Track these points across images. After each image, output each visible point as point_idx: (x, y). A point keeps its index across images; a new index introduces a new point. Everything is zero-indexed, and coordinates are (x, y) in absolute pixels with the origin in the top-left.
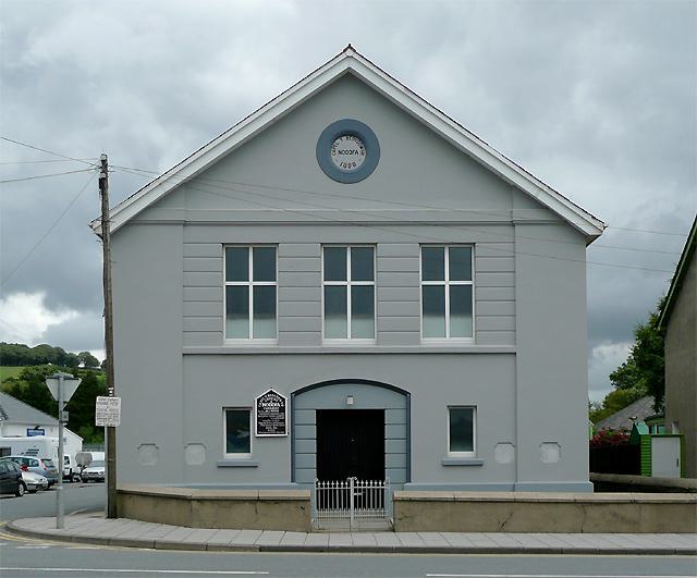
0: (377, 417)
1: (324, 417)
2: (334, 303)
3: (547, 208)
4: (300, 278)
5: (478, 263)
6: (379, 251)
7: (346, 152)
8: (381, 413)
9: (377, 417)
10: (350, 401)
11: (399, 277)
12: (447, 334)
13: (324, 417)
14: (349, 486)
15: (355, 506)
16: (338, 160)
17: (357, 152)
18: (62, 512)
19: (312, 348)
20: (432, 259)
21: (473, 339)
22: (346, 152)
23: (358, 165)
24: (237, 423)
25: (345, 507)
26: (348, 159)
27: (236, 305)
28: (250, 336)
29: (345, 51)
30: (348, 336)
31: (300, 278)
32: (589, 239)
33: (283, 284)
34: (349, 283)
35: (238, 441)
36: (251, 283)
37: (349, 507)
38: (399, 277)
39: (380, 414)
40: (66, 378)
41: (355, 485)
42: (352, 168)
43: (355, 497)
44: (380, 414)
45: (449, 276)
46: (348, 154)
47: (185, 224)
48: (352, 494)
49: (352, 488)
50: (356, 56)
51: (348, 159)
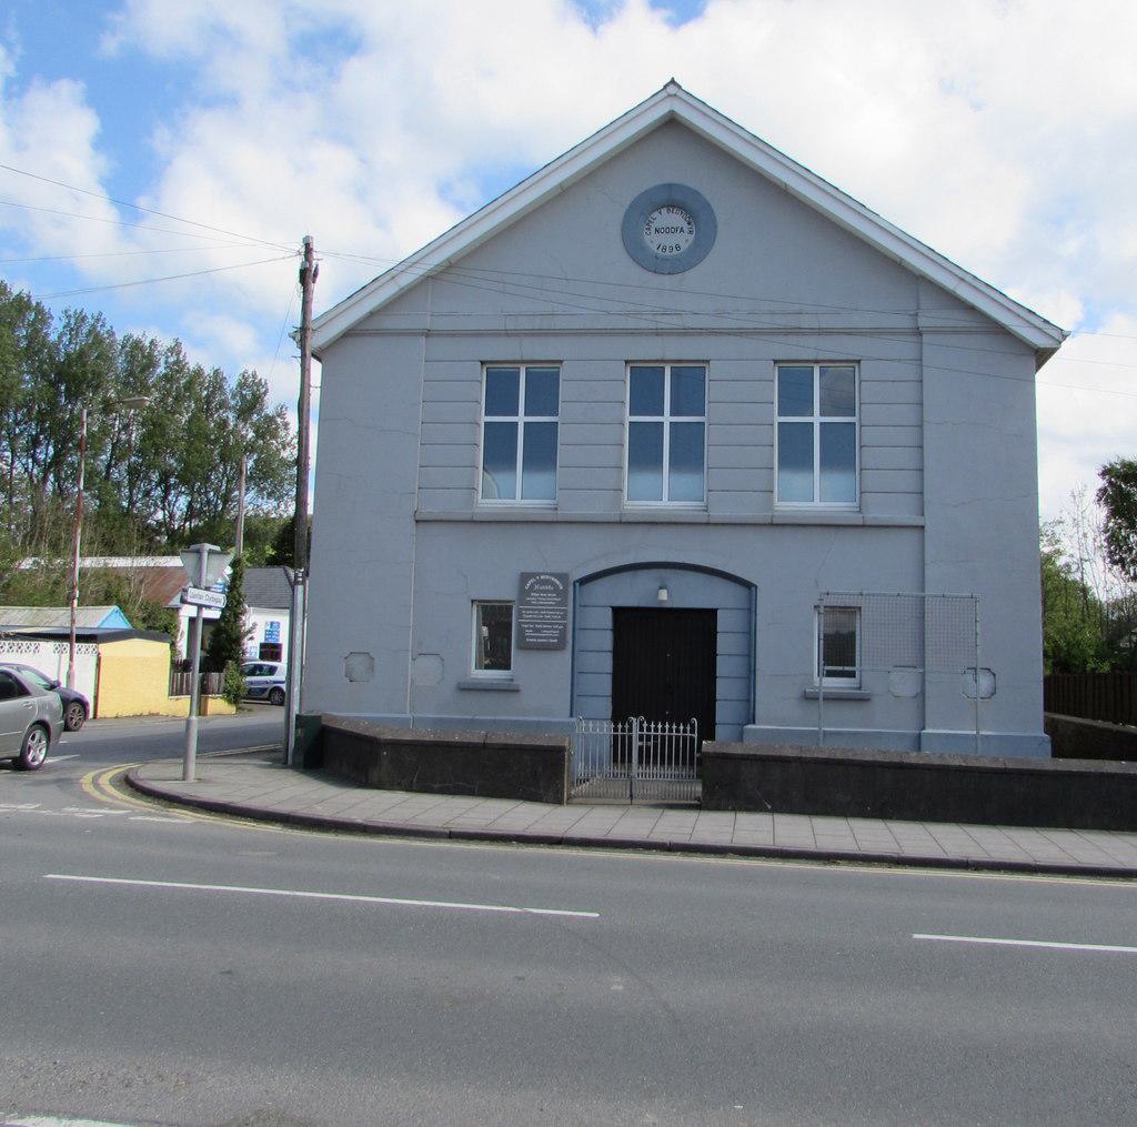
0: (706, 619)
1: (624, 618)
2: (644, 451)
3: (972, 309)
4: (595, 412)
5: (865, 393)
6: (712, 372)
7: (668, 230)
8: (714, 612)
9: (706, 619)
10: (663, 595)
11: (744, 404)
12: (815, 494)
13: (624, 618)
14: (630, 730)
15: (640, 762)
16: (652, 241)
17: (682, 230)
18: (923, 594)
19: (624, 509)
20: (645, 381)
21: (856, 504)
22: (668, 230)
23: (684, 247)
24: (497, 621)
25: (623, 761)
26: (670, 240)
27: (644, 451)
28: (518, 492)
29: (665, 87)
30: (665, 494)
31: (595, 412)
32: (1042, 356)
33: (569, 419)
34: (667, 419)
35: (496, 653)
36: (817, 419)
37: (630, 761)
38: (744, 404)
39: (711, 614)
40: (211, 552)
41: (641, 729)
42: (675, 252)
43: (641, 748)
44: (711, 614)
45: (819, 413)
46: (668, 232)
47: (428, 334)
48: (636, 744)
49: (636, 733)
50: (680, 94)
51: (670, 240)
